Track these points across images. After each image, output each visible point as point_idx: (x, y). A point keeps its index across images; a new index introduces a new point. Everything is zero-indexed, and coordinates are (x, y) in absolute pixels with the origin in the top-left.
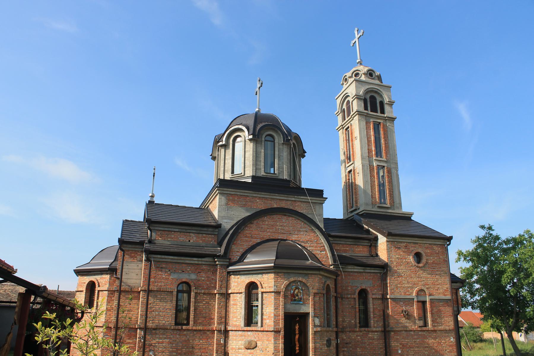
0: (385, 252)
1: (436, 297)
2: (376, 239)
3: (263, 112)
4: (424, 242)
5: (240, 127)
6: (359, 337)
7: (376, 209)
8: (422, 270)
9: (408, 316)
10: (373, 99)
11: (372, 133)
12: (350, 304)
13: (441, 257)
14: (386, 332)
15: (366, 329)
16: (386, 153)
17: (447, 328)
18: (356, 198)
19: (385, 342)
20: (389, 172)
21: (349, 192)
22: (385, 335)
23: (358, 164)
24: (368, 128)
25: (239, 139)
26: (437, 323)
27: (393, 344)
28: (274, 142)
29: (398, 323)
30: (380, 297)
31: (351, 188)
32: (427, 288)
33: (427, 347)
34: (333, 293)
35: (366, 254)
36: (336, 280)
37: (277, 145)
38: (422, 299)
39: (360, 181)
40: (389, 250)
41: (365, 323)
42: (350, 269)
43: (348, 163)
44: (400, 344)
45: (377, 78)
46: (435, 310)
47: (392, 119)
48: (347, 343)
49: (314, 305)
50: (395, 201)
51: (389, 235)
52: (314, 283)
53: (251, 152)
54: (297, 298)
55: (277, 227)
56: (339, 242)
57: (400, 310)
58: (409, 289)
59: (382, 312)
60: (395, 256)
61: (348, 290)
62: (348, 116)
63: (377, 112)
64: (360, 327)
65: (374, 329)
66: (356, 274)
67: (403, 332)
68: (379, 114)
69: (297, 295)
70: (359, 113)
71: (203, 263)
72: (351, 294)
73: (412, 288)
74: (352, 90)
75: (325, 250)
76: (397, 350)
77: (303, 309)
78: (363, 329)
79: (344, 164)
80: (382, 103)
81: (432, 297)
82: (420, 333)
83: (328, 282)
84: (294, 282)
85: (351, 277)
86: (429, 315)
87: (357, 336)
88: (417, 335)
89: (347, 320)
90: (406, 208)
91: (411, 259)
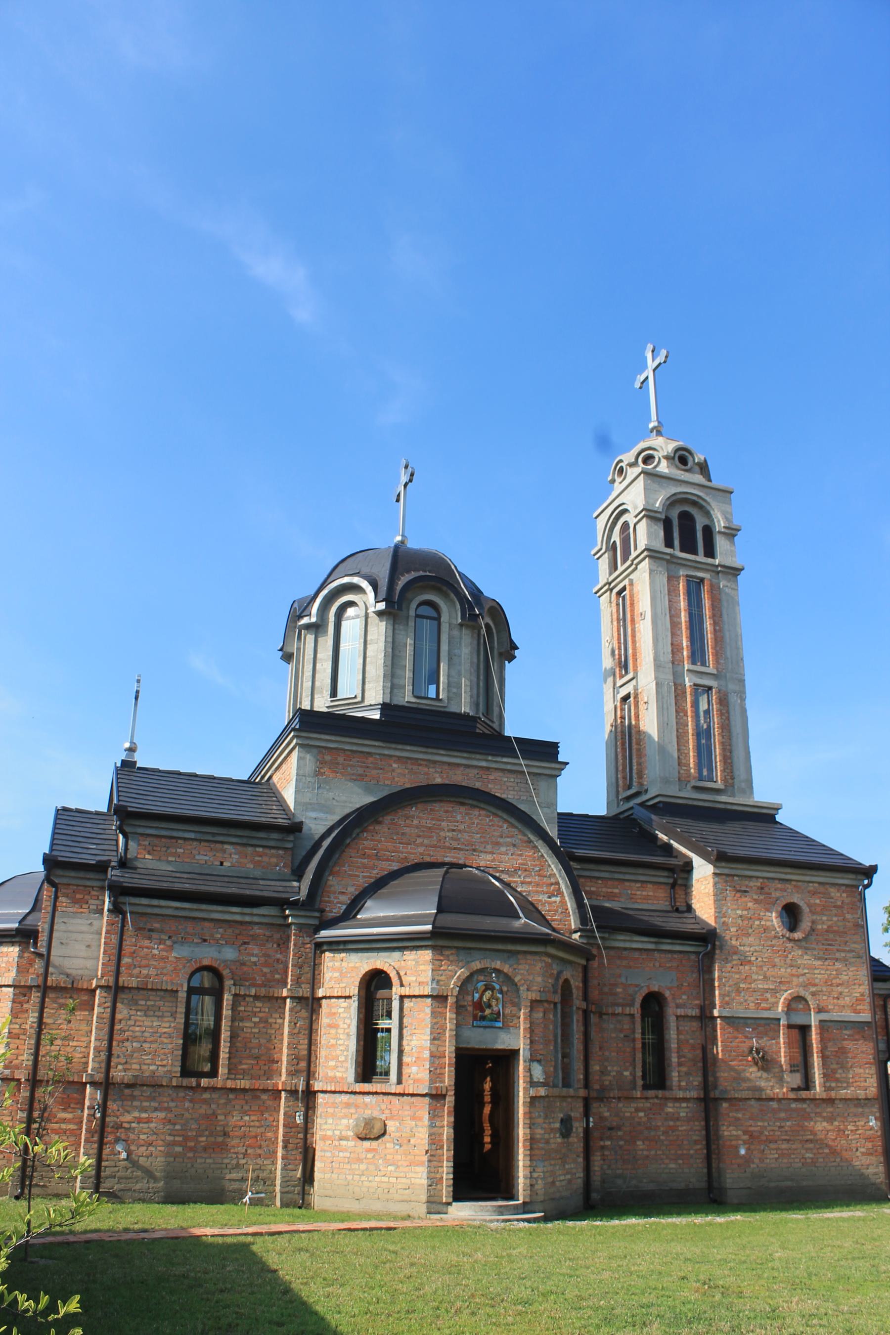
0: (710, 901)
1: (835, 1016)
2: (688, 867)
3: (413, 544)
4: (807, 878)
5: (356, 580)
6: (641, 1114)
7: (688, 793)
8: (800, 947)
9: (765, 1062)
10: (686, 519)
11: (683, 604)
12: (621, 1031)
13: (848, 916)
14: (709, 1103)
15: (660, 1093)
16: (717, 655)
17: (861, 1094)
18: (639, 764)
19: (707, 1128)
20: (723, 701)
21: (624, 749)
22: (707, 1111)
23: (646, 680)
24: (672, 592)
25: (351, 612)
26: (837, 1080)
27: (728, 1131)
28: (438, 619)
29: (739, 1078)
30: (695, 1012)
31: (626, 741)
32: (813, 994)
33: (811, 1141)
34: (578, 1002)
35: (664, 905)
36: (585, 969)
37: (445, 628)
38: (799, 1020)
39: (649, 723)
40: (719, 898)
41: (656, 1077)
42: (622, 941)
43: (622, 677)
44: (745, 1133)
45: (697, 468)
46: (832, 1048)
47: (734, 572)
48: (611, 1129)
49: (531, 1030)
50: (736, 773)
51: (720, 859)
52: (532, 975)
53: (382, 645)
55: (442, 834)
56: (596, 874)
57: (745, 1047)
58: (768, 995)
59: (699, 1052)
60: (735, 911)
61: (616, 994)
62: (624, 561)
63: (694, 552)
64: (645, 1087)
65: (681, 1094)
66: (636, 955)
67: (753, 1102)
68: (701, 558)
69: (490, 1006)
70: (652, 554)
71: (256, 919)
72: (623, 1005)
73: (775, 992)
74: (634, 496)
75: (559, 893)
76: (737, 1148)
77: (503, 1041)
78: (651, 1093)
79: (610, 680)
80: (708, 531)
81: (824, 1016)
82: (793, 1106)
83: (567, 974)
84: (481, 971)
85: (624, 963)
86: (816, 1060)
87: (637, 1110)
88: (786, 1111)
89: (613, 1069)
90: (763, 791)
91: (774, 919)
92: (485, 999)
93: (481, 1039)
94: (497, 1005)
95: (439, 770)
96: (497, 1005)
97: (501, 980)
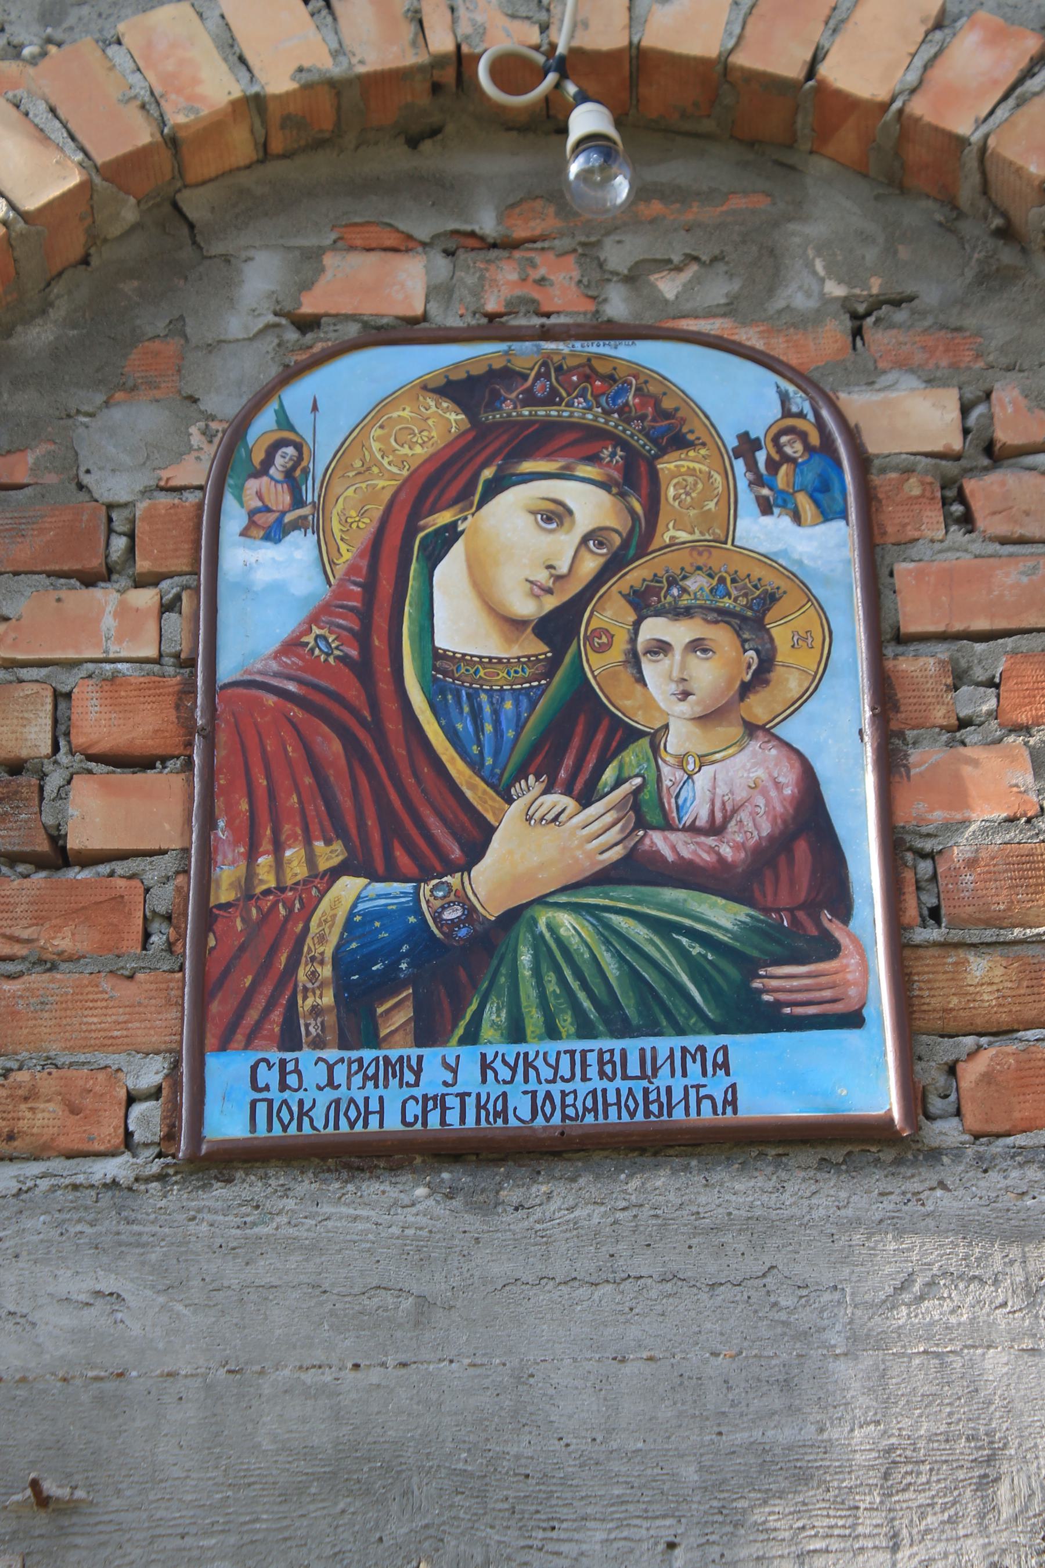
54: (535, 845)
69: (577, 736)
92: (458, 621)
94: (743, 708)
95: (912, 416)
96: (743, 708)
97: (814, 285)
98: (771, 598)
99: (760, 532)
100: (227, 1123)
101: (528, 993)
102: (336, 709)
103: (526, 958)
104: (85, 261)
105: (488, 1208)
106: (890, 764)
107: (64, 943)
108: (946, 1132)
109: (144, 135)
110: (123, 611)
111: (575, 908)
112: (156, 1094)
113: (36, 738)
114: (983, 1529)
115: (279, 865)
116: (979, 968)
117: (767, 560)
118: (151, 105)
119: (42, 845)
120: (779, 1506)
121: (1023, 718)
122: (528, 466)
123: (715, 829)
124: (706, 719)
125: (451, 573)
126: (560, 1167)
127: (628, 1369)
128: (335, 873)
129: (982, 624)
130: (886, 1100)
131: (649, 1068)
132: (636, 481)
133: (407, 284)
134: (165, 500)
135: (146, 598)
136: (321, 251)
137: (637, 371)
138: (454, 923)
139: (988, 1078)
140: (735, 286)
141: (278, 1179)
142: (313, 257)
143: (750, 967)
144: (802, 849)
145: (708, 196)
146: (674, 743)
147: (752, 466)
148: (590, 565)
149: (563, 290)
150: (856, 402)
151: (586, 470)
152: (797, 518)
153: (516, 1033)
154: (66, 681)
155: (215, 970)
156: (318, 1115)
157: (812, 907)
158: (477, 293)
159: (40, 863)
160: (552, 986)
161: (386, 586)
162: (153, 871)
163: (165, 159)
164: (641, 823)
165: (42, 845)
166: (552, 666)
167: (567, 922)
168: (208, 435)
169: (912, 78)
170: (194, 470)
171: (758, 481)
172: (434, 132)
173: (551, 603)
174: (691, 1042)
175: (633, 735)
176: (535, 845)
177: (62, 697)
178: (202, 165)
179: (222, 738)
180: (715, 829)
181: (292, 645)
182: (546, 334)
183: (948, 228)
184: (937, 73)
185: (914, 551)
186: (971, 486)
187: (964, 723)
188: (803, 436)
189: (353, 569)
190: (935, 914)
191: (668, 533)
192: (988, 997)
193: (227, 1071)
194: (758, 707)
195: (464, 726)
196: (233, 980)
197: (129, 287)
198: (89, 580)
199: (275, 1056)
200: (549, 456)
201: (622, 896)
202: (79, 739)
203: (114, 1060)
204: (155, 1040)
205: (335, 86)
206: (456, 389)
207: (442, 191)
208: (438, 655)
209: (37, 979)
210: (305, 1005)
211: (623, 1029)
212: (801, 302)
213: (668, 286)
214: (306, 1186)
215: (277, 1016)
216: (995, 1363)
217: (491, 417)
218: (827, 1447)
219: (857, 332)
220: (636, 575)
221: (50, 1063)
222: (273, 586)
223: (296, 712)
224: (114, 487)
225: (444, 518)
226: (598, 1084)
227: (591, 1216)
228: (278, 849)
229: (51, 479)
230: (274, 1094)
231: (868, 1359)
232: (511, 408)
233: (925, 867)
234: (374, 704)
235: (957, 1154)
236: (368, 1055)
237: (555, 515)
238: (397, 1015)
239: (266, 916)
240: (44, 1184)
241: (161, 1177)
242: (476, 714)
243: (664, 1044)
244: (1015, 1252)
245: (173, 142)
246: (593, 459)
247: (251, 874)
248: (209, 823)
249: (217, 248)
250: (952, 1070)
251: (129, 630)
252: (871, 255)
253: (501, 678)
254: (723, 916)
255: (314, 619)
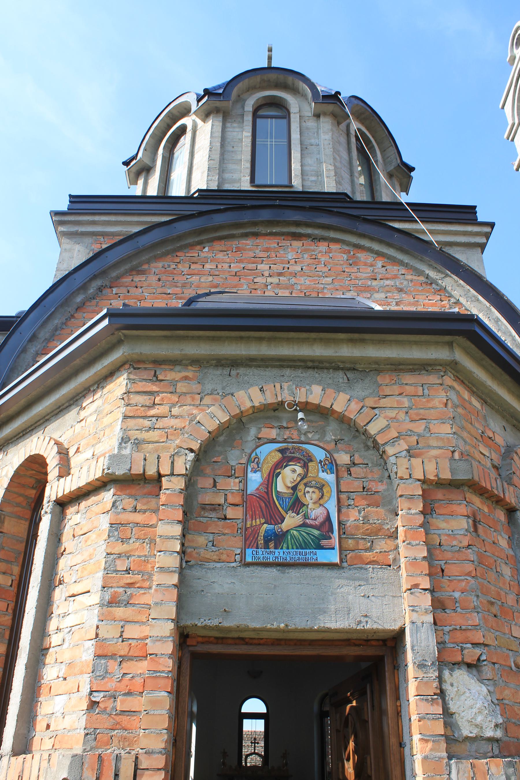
54: (291, 521)
69: (297, 505)
93: (260, 601)
94: (320, 502)
95: (343, 458)
96: (320, 502)
97: (330, 437)
98: (323, 485)
99: (323, 475)
100: (249, 559)
101: (289, 542)
102: (264, 499)
103: (289, 537)
104: (228, 427)
105: (284, 573)
106: (339, 511)
107: (226, 532)
108: (345, 564)
109: (238, 412)
110: (234, 482)
111: (296, 530)
112: (239, 554)
113: (222, 501)
114: (348, 620)
115: (256, 522)
116: (350, 541)
117: (323, 479)
118: (239, 407)
119: (223, 517)
120: (321, 616)
121: (357, 505)
122: (290, 463)
123: (315, 520)
124: (314, 503)
125: (279, 479)
126: (293, 567)
127: (302, 596)
128: (263, 524)
129: (352, 490)
130: (337, 560)
131: (306, 554)
132: (305, 466)
133: (273, 433)
134: (240, 465)
135: (237, 480)
136: (261, 428)
137: (306, 449)
138: (280, 532)
139: (351, 557)
140: (319, 436)
141: (256, 567)
142: (260, 428)
143: (320, 540)
144: (327, 523)
145: (316, 422)
146: (310, 507)
147: (321, 465)
148: (299, 479)
149: (295, 435)
150: (336, 455)
151: (298, 464)
152: (327, 473)
153: (288, 548)
154: (226, 492)
155: (247, 537)
156: (261, 558)
157: (328, 532)
158: (283, 435)
159: (223, 519)
160: (293, 542)
161: (271, 480)
162: (239, 521)
163: (241, 414)
164: (305, 518)
165: (223, 517)
166: (293, 494)
167: (295, 532)
168: (246, 455)
169: (345, 409)
170: (244, 461)
171: (322, 467)
172: (277, 409)
173: (293, 484)
174: (311, 551)
175: (304, 505)
176: (291, 521)
177: (226, 495)
178: (244, 415)
179: (248, 502)
180: (315, 520)
181: (257, 489)
182: (293, 443)
183: (349, 429)
184: (349, 408)
185: (343, 479)
186: (351, 469)
187: (349, 505)
188: (328, 461)
189: (266, 478)
190: (344, 533)
191: (309, 475)
192: (351, 546)
193: (249, 551)
194: (321, 502)
195: (281, 502)
196: (250, 539)
197: (234, 431)
198: (229, 477)
199: (255, 550)
200: (293, 462)
201: (302, 529)
202: (228, 502)
203: (233, 549)
204: (239, 546)
205: (265, 405)
206: (282, 451)
207: (278, 419)
208: (278, 492)
209: (223, 537)
210: (259, 543)
211: (302, 548)
212: (329, 439)
213: (310, 435)
214: (259, 568)
215: (256, 544)
216: (350, 597)
217: (285, 455)
218: (328, 608)
219: (336, 444)
220: (305, 481)
221: (225, 549)
222: (255, 480)
223: (258, 499)
224: (233, 463)
225: (279, 471)
226: (299, 556)
227: (298, 575)
228: (256, 520)
229: (224, 461)
230: (255, 555)
231: (334, 596)
232: (288, 454)
233: (343, 526)
234: (269, 498)
235: (346, 568)
236: (268, 550)
237: (294, 471)
238: (272, 544)
239: (254, 529)
240: (224, 566)
241: (240, 566)
242: (283, 501)
243: (308, 551)
244: (353, 582)
245: (242, 412)
246: (299, 463)
247: (252, 523)
248: (246, 515)
249: (247, 426)
250: (346, 556)
251: (235, 486)
252: (338, 432)
253: (286, 496)
254: (316, 532)
255: (260, 485)
